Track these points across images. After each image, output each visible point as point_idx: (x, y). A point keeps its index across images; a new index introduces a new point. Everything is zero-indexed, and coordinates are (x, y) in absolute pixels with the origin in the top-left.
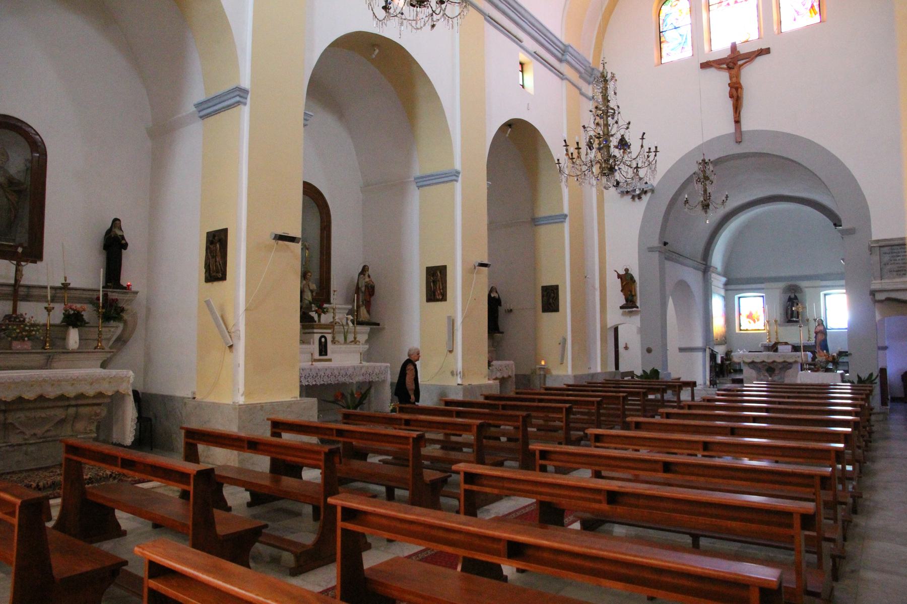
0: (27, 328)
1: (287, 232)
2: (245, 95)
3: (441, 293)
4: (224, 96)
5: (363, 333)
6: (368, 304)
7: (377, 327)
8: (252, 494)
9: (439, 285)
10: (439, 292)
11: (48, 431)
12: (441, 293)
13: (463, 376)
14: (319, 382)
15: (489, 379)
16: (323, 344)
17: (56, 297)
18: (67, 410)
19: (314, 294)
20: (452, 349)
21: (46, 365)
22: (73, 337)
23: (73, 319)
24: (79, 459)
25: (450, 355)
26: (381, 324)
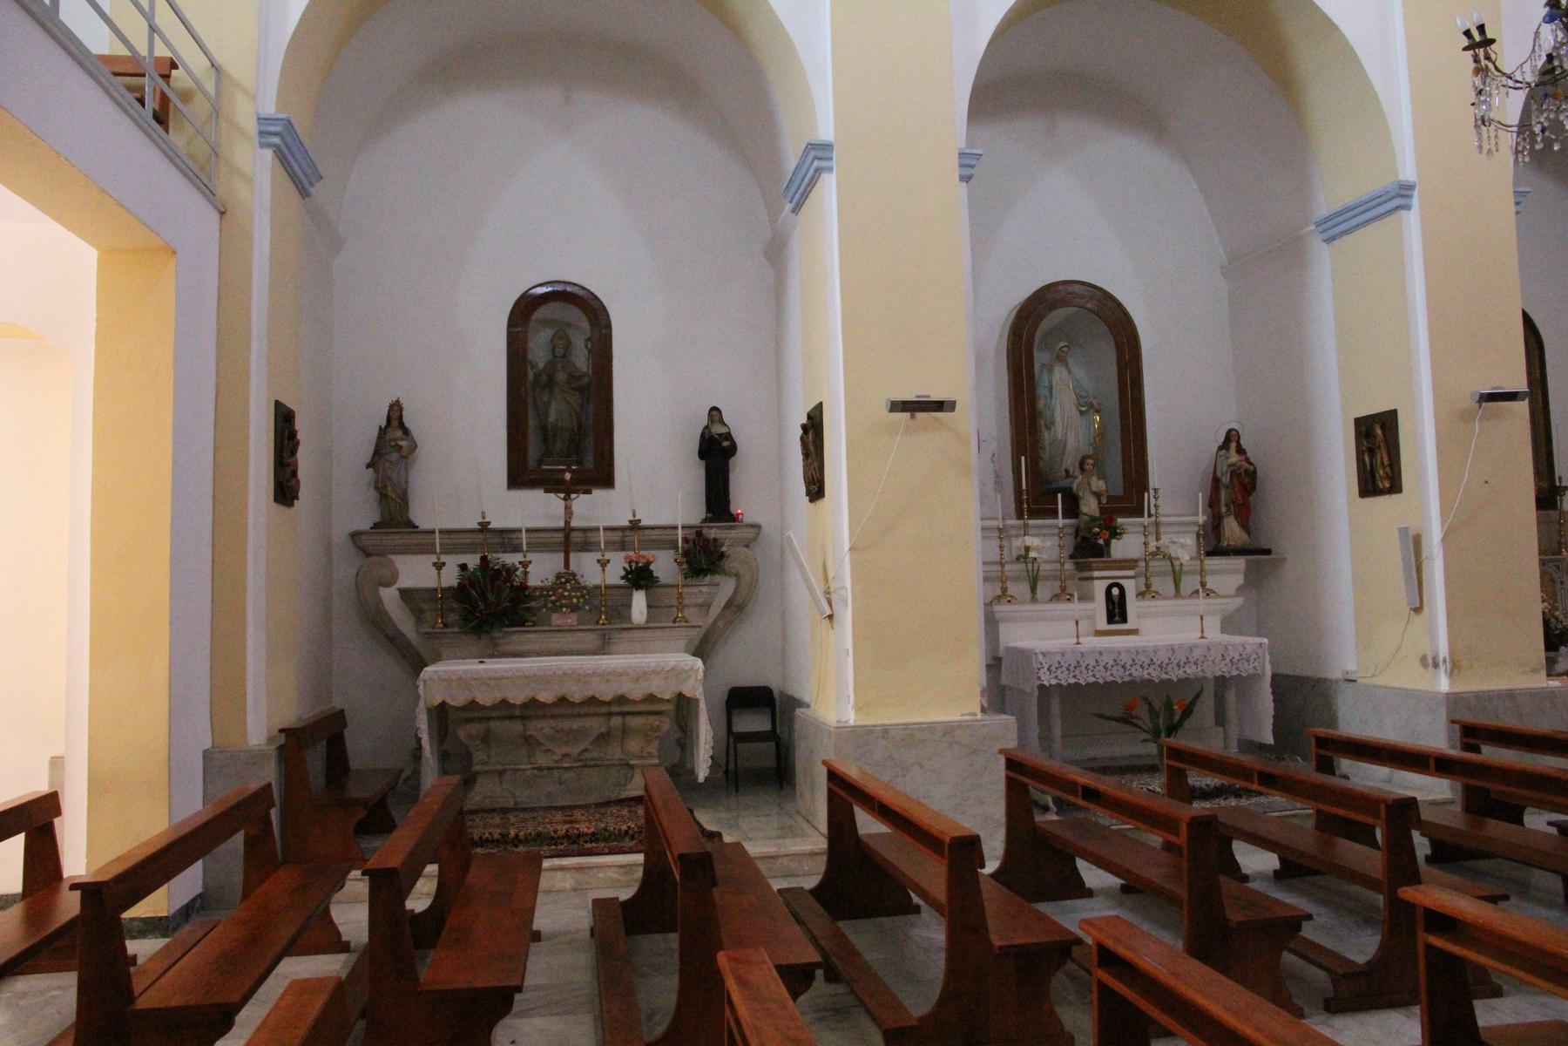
0: (566, 594)
1: (924, 394)
2: (828, 154)
3: (1388, 476)
4: (803, 162)
5: (1228, 574)
6: (1244, 513)
7: (1267, 557)
8: (1282, 860)
9: (1383, 456)
10: (1381, 472)
11: (585, 750)
12: (1388, 476)
13: (1455, 668)
14: (1085, 678)
15: (1549, 675)
16: (1116, 600)
17: (625, 542)
18: (609, 720)
19: (1104, 501)
20: (1418, 605)
21: (604, 648)
22: (639, 600)
23: (640, 577)
24: (1182, 766)
25: (1417, 619)
26: (1273, 550)
